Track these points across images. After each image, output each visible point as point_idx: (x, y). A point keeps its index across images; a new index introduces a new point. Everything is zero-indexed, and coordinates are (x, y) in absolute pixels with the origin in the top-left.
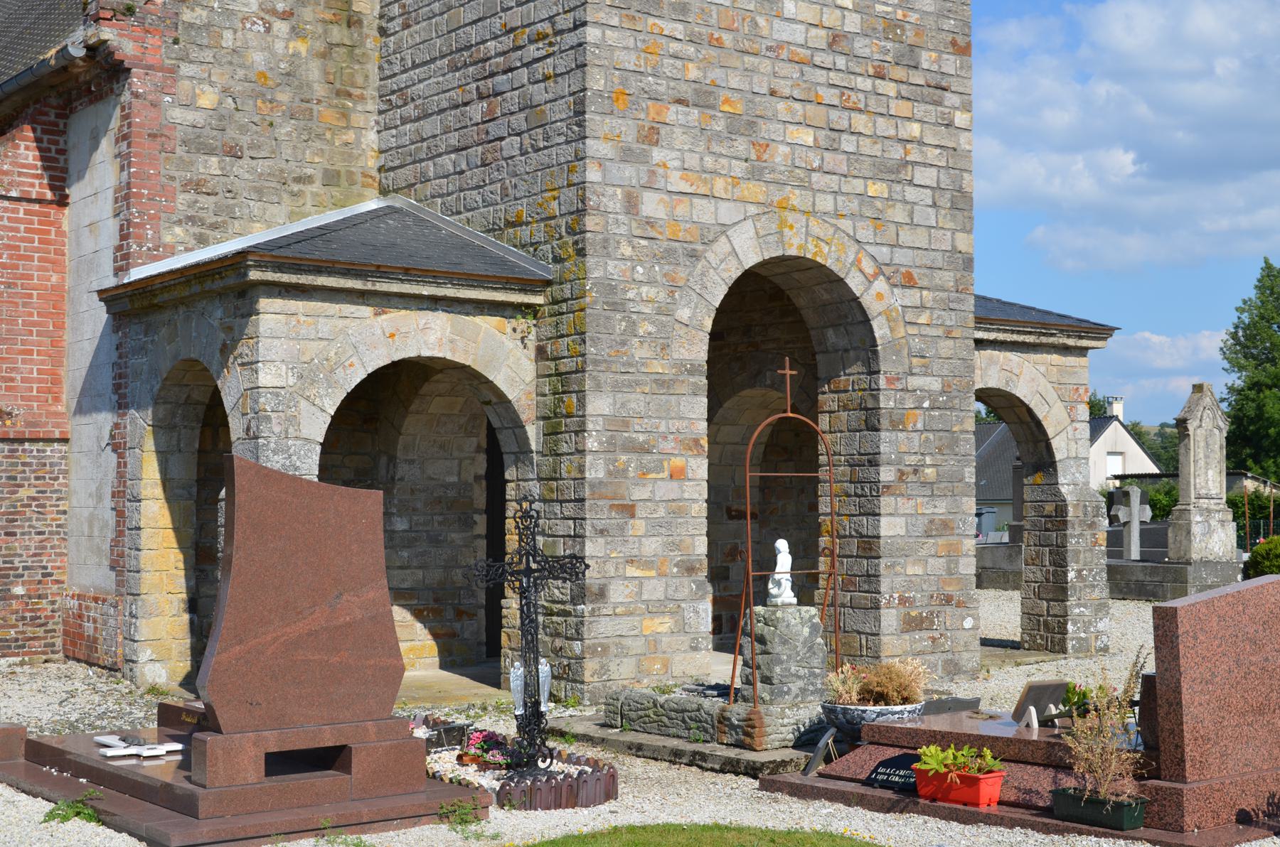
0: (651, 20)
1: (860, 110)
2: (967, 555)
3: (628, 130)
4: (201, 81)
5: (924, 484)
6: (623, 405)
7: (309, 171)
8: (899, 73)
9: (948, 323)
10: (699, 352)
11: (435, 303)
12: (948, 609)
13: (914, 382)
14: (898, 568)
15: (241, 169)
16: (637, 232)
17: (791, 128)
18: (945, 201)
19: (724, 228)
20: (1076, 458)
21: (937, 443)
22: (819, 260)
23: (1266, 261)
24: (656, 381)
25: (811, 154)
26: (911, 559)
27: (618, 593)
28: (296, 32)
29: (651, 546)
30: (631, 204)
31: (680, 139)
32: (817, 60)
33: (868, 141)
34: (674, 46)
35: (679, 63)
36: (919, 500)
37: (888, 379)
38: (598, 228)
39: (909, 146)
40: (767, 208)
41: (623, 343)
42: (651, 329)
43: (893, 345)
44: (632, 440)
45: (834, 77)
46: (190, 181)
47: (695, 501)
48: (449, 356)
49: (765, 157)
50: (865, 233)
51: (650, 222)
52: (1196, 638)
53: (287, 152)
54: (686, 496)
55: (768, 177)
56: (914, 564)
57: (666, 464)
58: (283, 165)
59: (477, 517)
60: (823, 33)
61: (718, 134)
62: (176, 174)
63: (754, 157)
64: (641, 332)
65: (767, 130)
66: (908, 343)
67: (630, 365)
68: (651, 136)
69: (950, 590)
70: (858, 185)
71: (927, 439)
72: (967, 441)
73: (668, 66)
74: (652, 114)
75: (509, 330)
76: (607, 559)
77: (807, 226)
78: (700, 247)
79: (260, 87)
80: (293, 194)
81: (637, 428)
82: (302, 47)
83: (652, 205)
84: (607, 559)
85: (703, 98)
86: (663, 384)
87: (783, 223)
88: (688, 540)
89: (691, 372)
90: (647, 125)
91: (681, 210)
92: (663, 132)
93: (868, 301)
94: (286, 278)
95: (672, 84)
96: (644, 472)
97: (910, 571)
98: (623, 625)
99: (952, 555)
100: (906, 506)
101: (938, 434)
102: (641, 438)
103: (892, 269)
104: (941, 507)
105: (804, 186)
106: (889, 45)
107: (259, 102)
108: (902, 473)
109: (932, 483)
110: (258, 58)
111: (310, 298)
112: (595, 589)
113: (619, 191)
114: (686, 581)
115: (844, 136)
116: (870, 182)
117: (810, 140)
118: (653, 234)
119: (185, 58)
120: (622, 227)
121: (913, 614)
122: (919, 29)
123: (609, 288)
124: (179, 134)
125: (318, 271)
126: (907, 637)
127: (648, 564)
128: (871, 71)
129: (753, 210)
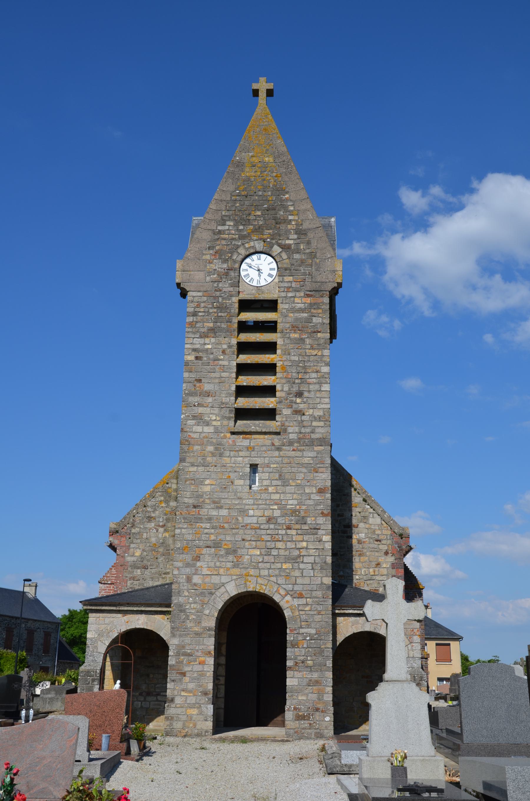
0: (198, 524)
1: (280, 541)
2: (327, 693)
3: (188, 558)
4: (136, 548)
5: (307, 667)
6: (183, 641)
7: (168, 571)
8: (298, 526)
9: (319, 609)
10: (212, 623)
11: (141, 612)
12: (317, 713)
13: (302, 631)
14: (295, 697)
15: (147, 572)
16: (191, 588)
17: (250, 550)
18: (318, 567)
19: (223, 584)
20: (413, 657)
21: (313, 652)
22: (261, 591)
23: (80, 602)
24: (195, 633)
25: (259, 558)
26: (300, 694)
27: (178, 700)
28: (166, 531)
29: (191, 686)
30: (189, 579)
31: (207, 558)
32: (262, 527)
33: (283, 550)
34: (206, 531)
35: (207, 536)
36: (304, 673)
37: (291, 630)
38: (176, 588)
39: (301, 550)
40: (241, 576)
41: (184, 622)
42: (194, 617)
43: (293, 618)
44: (185, 652)
45: (269, 532)
46: (132, 577)
47: (208, 671)
48: (145, 627)
49: (240, 560)
50: (281, 581)
51: (195, 585)
52: (72, 703)
53: (161, 566)
54: (205, 670)
55: (241, 566)
56: (302, 695)
57: (197, 660)
58: (160, 570)
59: (221, 678)
60: (264, 518)
61: (222, 555)
62: (128, 576)
63: (235, 561)
64: (190, 618)
65: (240, 552)
66: (300, 617)
67: (186, 629)
68: (197, 558)
69: (319, 706)
70: (279, 565)
71: (309, 651)
72: (328, 651)
73: (204, 537)
74: (197, 552)
75: (166, 619)
76: (174, 689)
77: (257, 581)
78: (214, 591)
79: (154, 548)
80: (163, 578)
81: (187, 648)
82: (167, 535)
83: (196, 579)
84: (174, 689)
85: (217, 545)
86: (197, 634)
87: (246, 580)
88: (205, 684)
89: (209, 630)
90: (195, 556)
91: (207, 580)
92: (201, 557)
93: (283, 604)
94: (93, 608)
95: (205, 542)
96: (189, 662)
97: (300, 698)
98: (179, 711)
99: (321, 693)
100: (297, 674)
101: (313, 649)
102: (189, 651)
103: (293, 592)
104: (315, 675)
105: (256, 568)
106: (293, 518)
107: (153, 552)
108: (297, 663)
109: (311, 667)
110: (153, 540)
111: (103, 613)
112: (170, 699)
113: (184, 576)
114: (204, 697)
115: (273, 550)
116: (283, 564)
117: (258, 553)
118: (196, 588)
119: (132, 543)
120: (185, 586)
121: (300, 714)
122: (306, 511)
123: (180, 605)
124: (129, 564)
125: (102, 605)
126: (297, 722)
127: (190, 692)
128: (285, 527)
129: (235, 577)
